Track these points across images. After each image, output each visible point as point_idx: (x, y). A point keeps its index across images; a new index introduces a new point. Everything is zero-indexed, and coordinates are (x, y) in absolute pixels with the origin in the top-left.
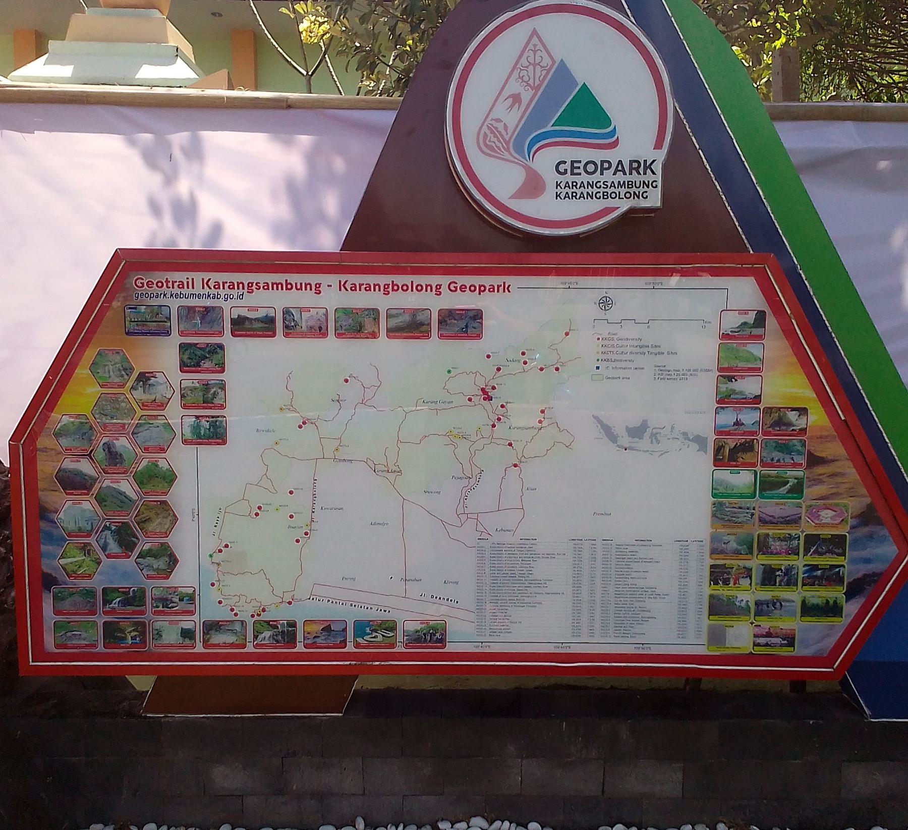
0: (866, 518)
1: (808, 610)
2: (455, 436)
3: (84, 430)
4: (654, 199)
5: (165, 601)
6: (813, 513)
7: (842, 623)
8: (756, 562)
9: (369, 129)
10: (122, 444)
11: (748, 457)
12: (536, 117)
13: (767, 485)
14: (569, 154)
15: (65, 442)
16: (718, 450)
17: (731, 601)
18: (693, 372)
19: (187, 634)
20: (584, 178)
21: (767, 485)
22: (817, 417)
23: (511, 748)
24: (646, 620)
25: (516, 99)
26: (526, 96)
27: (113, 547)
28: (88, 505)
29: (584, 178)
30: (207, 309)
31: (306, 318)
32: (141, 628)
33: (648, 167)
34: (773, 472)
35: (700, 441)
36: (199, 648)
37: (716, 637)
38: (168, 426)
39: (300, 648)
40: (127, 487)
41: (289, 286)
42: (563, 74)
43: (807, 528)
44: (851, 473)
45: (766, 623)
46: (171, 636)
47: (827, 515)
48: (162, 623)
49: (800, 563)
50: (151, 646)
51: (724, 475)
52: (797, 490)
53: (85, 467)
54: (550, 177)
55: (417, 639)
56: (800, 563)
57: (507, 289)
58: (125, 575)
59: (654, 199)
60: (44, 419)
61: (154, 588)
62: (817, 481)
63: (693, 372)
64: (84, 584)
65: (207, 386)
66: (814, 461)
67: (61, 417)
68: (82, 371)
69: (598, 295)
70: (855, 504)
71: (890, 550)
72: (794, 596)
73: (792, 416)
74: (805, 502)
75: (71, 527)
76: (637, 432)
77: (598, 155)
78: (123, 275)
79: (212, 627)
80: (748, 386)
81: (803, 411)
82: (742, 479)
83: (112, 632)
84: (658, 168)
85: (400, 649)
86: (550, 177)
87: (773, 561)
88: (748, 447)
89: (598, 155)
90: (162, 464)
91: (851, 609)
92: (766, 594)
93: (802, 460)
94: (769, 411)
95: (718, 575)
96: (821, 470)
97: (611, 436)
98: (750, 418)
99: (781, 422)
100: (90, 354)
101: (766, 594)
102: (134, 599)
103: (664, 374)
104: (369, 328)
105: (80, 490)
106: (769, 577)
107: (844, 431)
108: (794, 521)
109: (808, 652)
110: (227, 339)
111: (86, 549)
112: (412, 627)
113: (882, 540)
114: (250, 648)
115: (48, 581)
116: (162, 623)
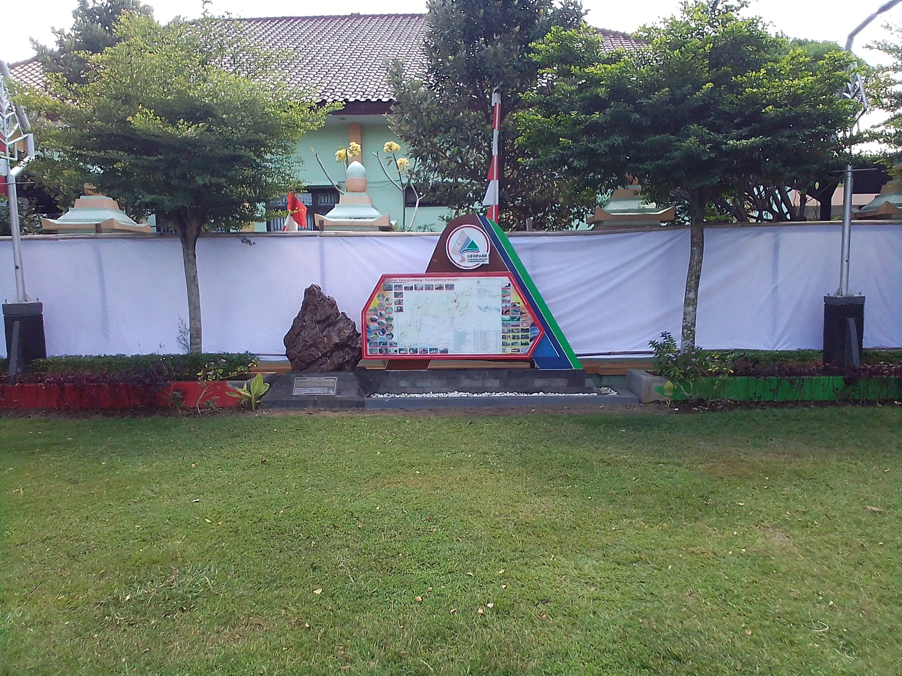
0: (532, 325)
1: (522, 344)
2: (449, 309)
3: (375, 310)
4: (487, 262)
5: (391, 344)
6: (522, 324)
7: (530, 346)
8: (511, 334)
9: (433, 241)
10: (383, 312)
11: (509, 313)
12: (464, 246)
13: (513, 319)
14: (470, 254)
15: (372, 312)
16: (503, 311)
17: (506, 343)
18: (496, 296)
19: (396, 351)
20: (473, 258)
21: (513, 319)
22: (522, 304)
23: (463, 377)
24: (489, 347)
25: (460, 244)
26: (461, 243)
27: (381, 333)
28: (376, 325)
29: (473, 258)
30: (400, 285)
31: (419, 287)
32: (387, 350)
33: (486, 256)
34: (514, 316)
35: (499, 310)
36: (398, 354)
37: (504, 350)
38: (392, 309)
39: (418, 354)
40: (384, 321)
41: (416, 280)
42: (468, 239)
43: (521, 327)
44: (529, 316)
45: (514, 347)
46: (392, 352)
47: (525, 324)
48: (390, 349)
49: (520, 334)
50: (389, 354)
51: (504, 316)
52: (519, 320)
53: (376, 317)
54: (467, 258)
55: (442, 352)
56: (520, 334)
57: (458, 279)
58: (384, 339)
59: (487, 262)
60: (368, 308)
61: (389, 341)
62: (522, 317)
63: (496, 296)
64: (376, 341)
65: (399, 300)
66: (522, 313)
67: (372, 307)
68: (375, 298)
69: (477, 281)
70: (531, 322)
71: (538, 331)
72: (519, 341)
73: (517, 304)
74: (520, 322)
75: (373, 329)
76: (486, 308)
77: (476, 254)
78: (384, 279)
79: (400, 350)
80: (507, 298)
81: (519, 303)
82: (508, 317)
83: (381, 351)
84: (488, 256)
85: (439, 354)
86: (467, 258)
87: (514, 334)
88: (509, 311)
89: (476, 254)
90: (391, 316)
91: (531, 344)
92: (514, 341)
93: (519, 313)
94: (512, 303)
95: (503, 337)
96: (523, 315)
97: (481, 309)
98: (508, 305)
99: (515, 306)
100: (377, 295)
101: (514, 341)
102: (385, 344)
103: (490, 296)
104: (431, 288)
105: (337, 386)
106: (514, 338)
107: (527, 306)
108: (519, 326)
109: (523, 353)
110: (403, 291)
111: (376, 334)
112: (441, 349)
113: (536, 329)
114: (408, 354)
115: (368, 340)
116: (390, 349)
